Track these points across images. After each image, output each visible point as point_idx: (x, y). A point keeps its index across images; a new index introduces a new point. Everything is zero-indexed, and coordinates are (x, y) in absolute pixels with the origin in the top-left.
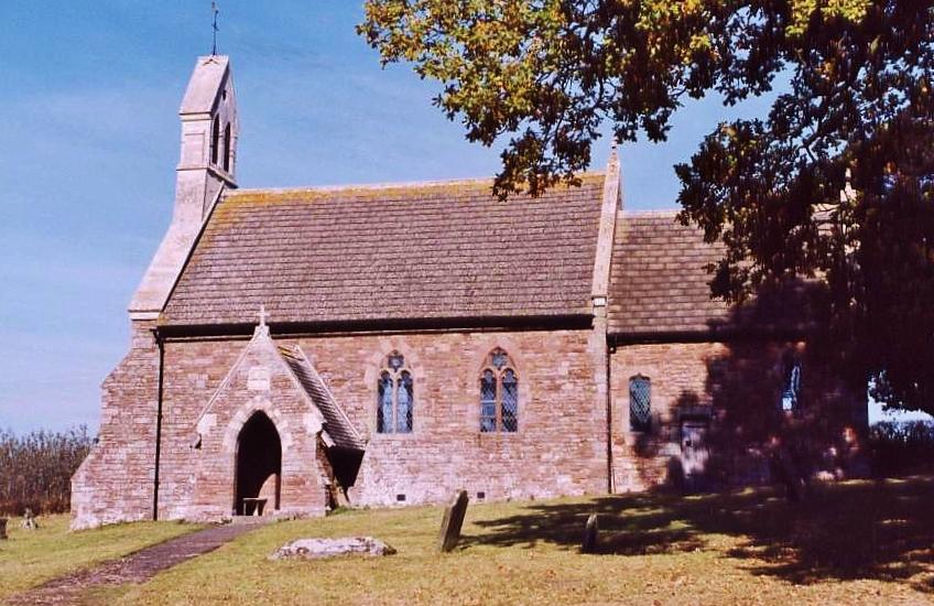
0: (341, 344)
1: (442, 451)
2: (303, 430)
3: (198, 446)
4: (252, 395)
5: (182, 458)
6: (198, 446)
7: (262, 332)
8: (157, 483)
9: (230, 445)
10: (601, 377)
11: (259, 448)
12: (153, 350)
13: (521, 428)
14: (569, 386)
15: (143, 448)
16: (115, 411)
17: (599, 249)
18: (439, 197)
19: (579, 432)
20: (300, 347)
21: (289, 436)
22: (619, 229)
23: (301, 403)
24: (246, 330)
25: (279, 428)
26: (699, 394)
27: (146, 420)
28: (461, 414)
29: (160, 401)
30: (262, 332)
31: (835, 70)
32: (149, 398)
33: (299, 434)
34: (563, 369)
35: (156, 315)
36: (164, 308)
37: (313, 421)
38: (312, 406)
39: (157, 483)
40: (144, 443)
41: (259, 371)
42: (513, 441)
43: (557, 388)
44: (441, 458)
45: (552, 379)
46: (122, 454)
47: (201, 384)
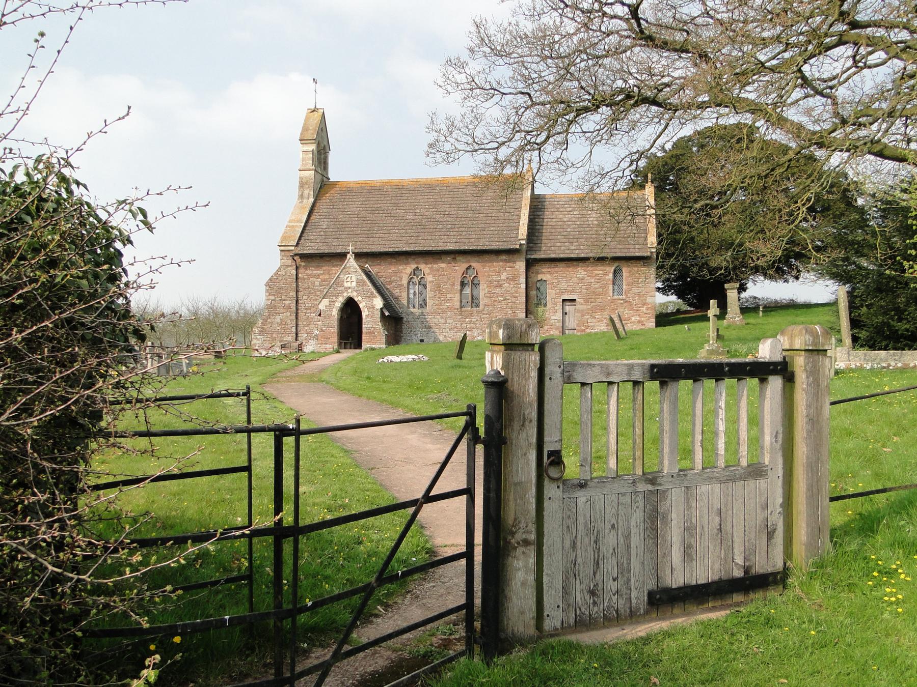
0: (531, 405)
1: (442, 317)
2: (373, 307)
3: (320, 315)
4: (347, 289)
5: (310, 322)
6: (320, 315)
7: (351, 258)
8: (297, 334)
9: (335, 313)
10: (523, 280)
11: (351, 314)
12: (291, 266)
13: (481, 306)
14: (507, 285)
15: (289, 317)
16: (273, 298)
17: (522, 215)
18: (438, 186)
19: (511, 308)
20: (381, 270)
21: (366, 310)
22: (112, 494)
23: (372, 293)
24: (342, 256)
25: (361, 306)
26: (164, 278)
27: (290, 301)
28: (451, 300)
29: (297, 292)
30: (351, 258)
31: (18, 570)
32: (288, 290)
33: (372, 308)
34: (503, 277)
35: (293, 248)
36: (298, 243)
37: (379, 303)
38: (377, 295)
39: (297, 334)
40: (289, 314)
41: (351, 280)
42: (478, 312)
43: (501, 286)
44: (442, 321)
45: (498, 281)
46: (278, 319)
47: (317, 283)
